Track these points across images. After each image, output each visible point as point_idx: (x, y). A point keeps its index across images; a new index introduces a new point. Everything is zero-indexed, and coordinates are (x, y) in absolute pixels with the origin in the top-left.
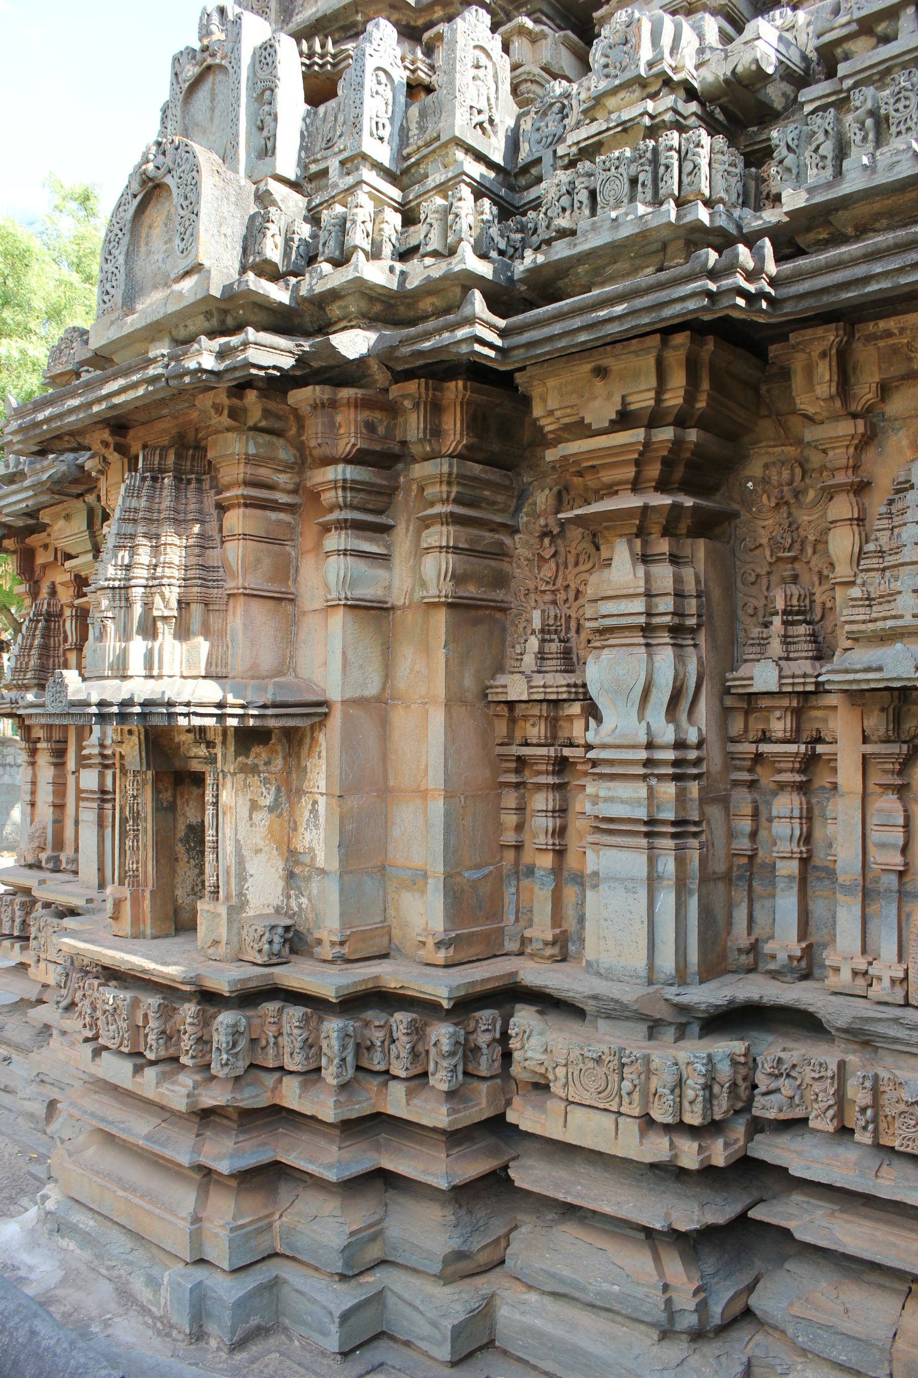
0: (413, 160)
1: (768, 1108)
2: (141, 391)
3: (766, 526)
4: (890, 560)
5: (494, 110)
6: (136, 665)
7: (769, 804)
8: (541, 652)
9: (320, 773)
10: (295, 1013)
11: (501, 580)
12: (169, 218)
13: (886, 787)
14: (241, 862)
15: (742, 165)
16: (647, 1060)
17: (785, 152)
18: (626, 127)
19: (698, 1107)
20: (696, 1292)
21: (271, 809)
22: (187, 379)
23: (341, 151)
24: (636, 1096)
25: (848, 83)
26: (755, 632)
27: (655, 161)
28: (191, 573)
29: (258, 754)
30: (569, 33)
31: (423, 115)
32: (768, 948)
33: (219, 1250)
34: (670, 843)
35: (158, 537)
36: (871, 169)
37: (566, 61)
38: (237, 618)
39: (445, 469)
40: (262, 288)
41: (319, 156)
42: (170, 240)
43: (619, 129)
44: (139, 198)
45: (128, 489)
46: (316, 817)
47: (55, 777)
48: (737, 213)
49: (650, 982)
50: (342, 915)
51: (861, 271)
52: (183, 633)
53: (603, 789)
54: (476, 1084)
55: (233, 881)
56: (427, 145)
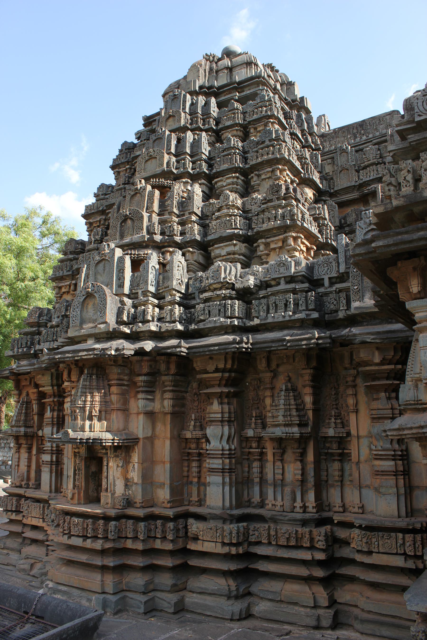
1: (253, 539)
2: (92, 356)
3: (251, 394)
4: (278, 408)
6: (87, 428)
7: (252, 464)
8: (195, 425)
9: (135, 458)
10: (131, 522)
11: (183, 405)
13: (278, 460)
14: (114, 481)
16: (223, 528)
19: (236, 538)
20: (236, 586)
21: (122, 467)
22: (107, 356)
24: (220, 537)
26: (248, 421)
28: (102, 403)
29: (119, 452)
31: (164, 278)
32: (252, 500)
33: (110, 589)
34: (228, 474)
35: (93, 393)
36: (274, 317)
38: (114, 416)
39: (171, 378)
44: (85, 296)
45: (83, 379)
46: (134, 469)
47: (28, 456)
48: (244, 320)
49: (223, 509)
50: (142, 495)
51: (270, 344)
52: (100, 420)
53: (211, 461)
54: (179, 539)
55: (112, 486)
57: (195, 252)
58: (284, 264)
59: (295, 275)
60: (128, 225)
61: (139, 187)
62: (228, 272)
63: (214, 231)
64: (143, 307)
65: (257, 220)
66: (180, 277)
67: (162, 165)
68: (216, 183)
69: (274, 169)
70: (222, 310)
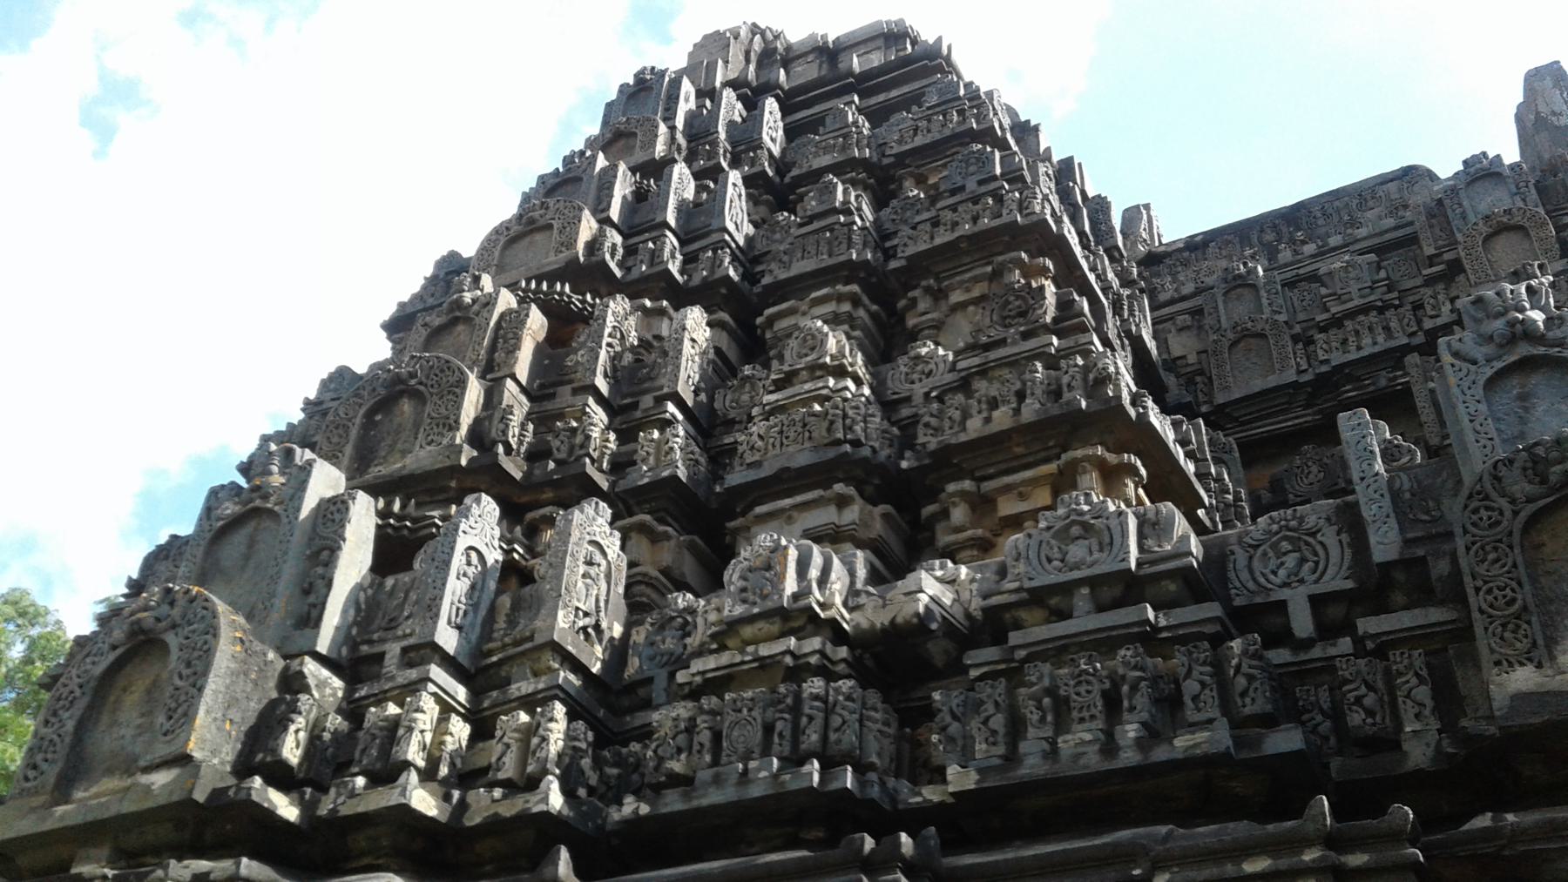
0: (494, 659)
5: (602, 614)
12: (155, 685)
15: (895, 725)
17: (948, 719)
18: (765, 664)
23: (405, 636)
25: (1022, 653)
27: (796, 709)
30: (696, 538)
31: (516, 606)
37: (689, 568)
40: (270, 801)
41: (375, 636)
42: (150, 713)
43: (755, 665)
44: (119, 651)
48: (891, 782)
56: (517, 643)
57: (667, 537)
58: (1087, 527)
59: (1148, 570)
60: (397, 420)
61: (468, 297)
62: (814, 573)
63: (757, 457)
64: (392, 709)
65: (939, 415)
66: (589, 606)
67: (571, 243)
68: (771, 321)
69: (1002, 264)
70: (779, 726)
